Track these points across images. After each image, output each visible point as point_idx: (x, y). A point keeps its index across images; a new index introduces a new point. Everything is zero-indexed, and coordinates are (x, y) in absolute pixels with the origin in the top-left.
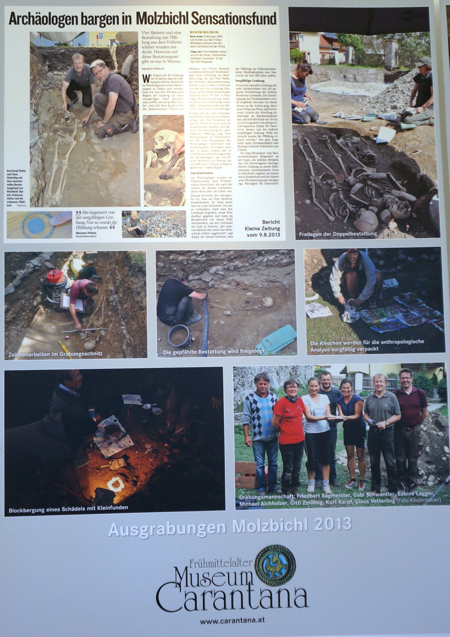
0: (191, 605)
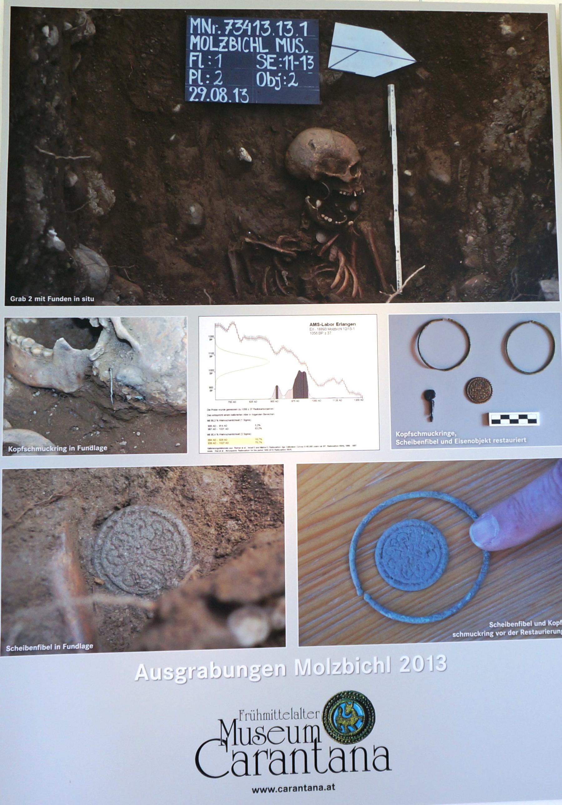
0: (240, 768)
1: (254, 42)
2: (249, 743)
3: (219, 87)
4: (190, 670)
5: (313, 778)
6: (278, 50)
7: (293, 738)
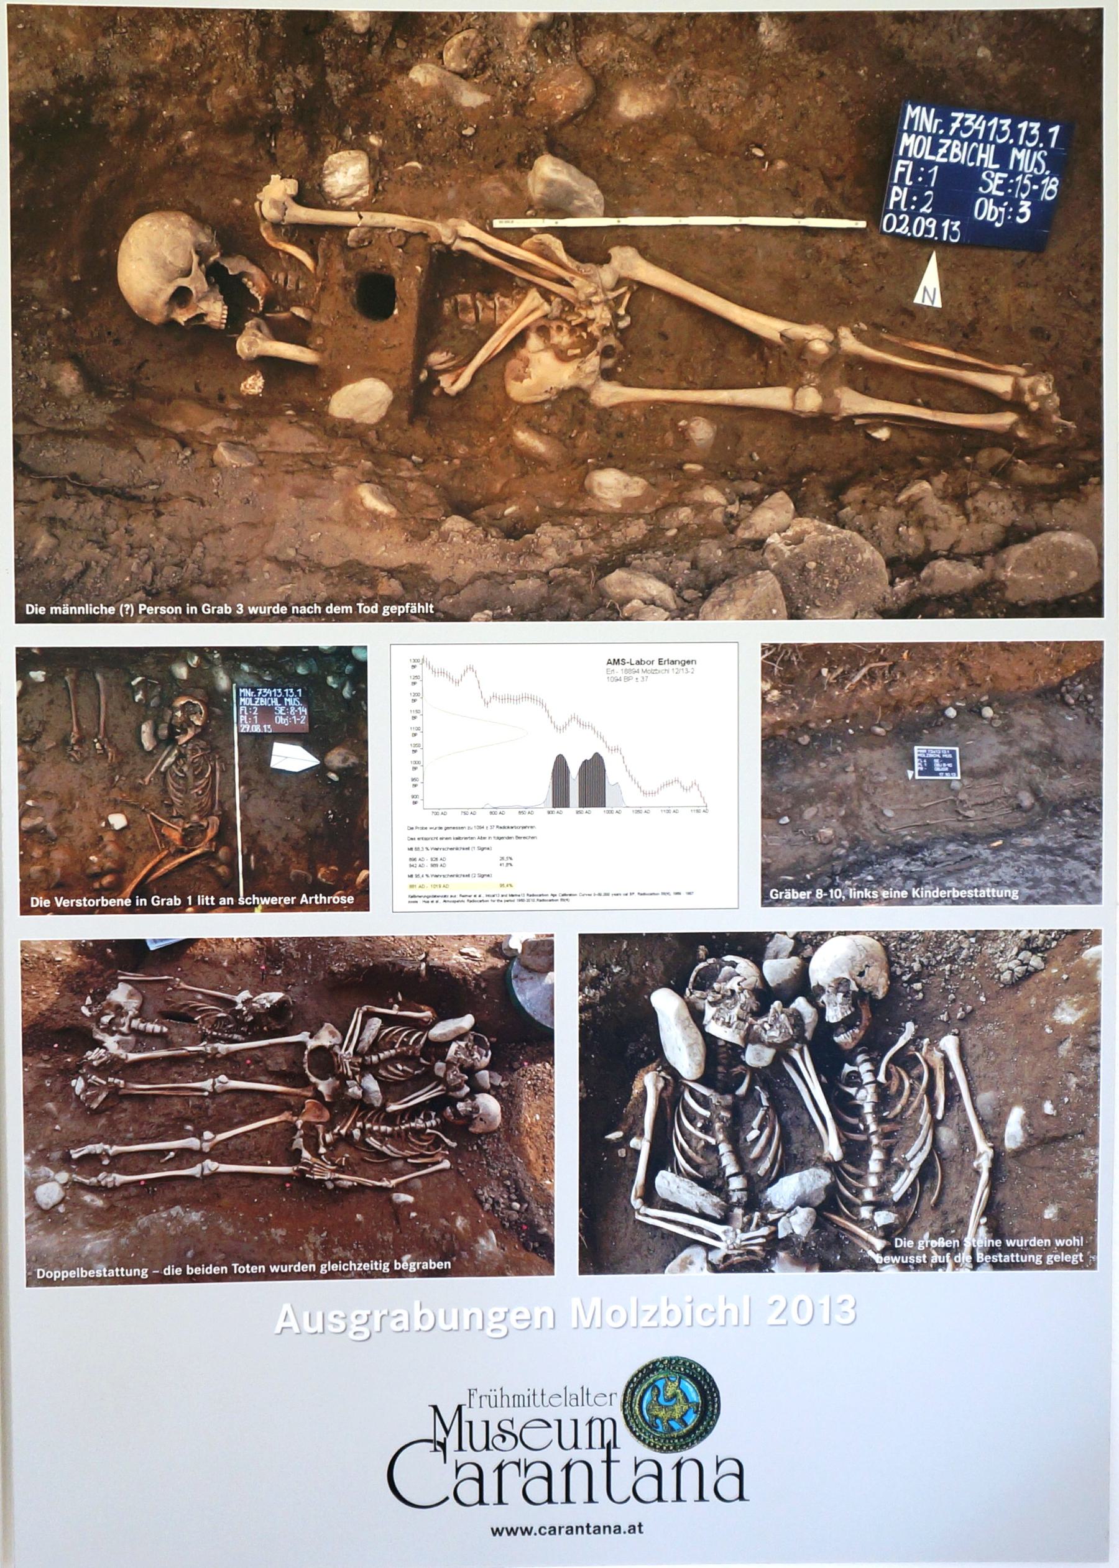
0: (469, 1492)
1: (984, 152)
2: (487, 1447)
3: (926, 216)
4: (377, 1316)
5: (603, 1512)
6: (1011, 167)
7: (568, 1441)
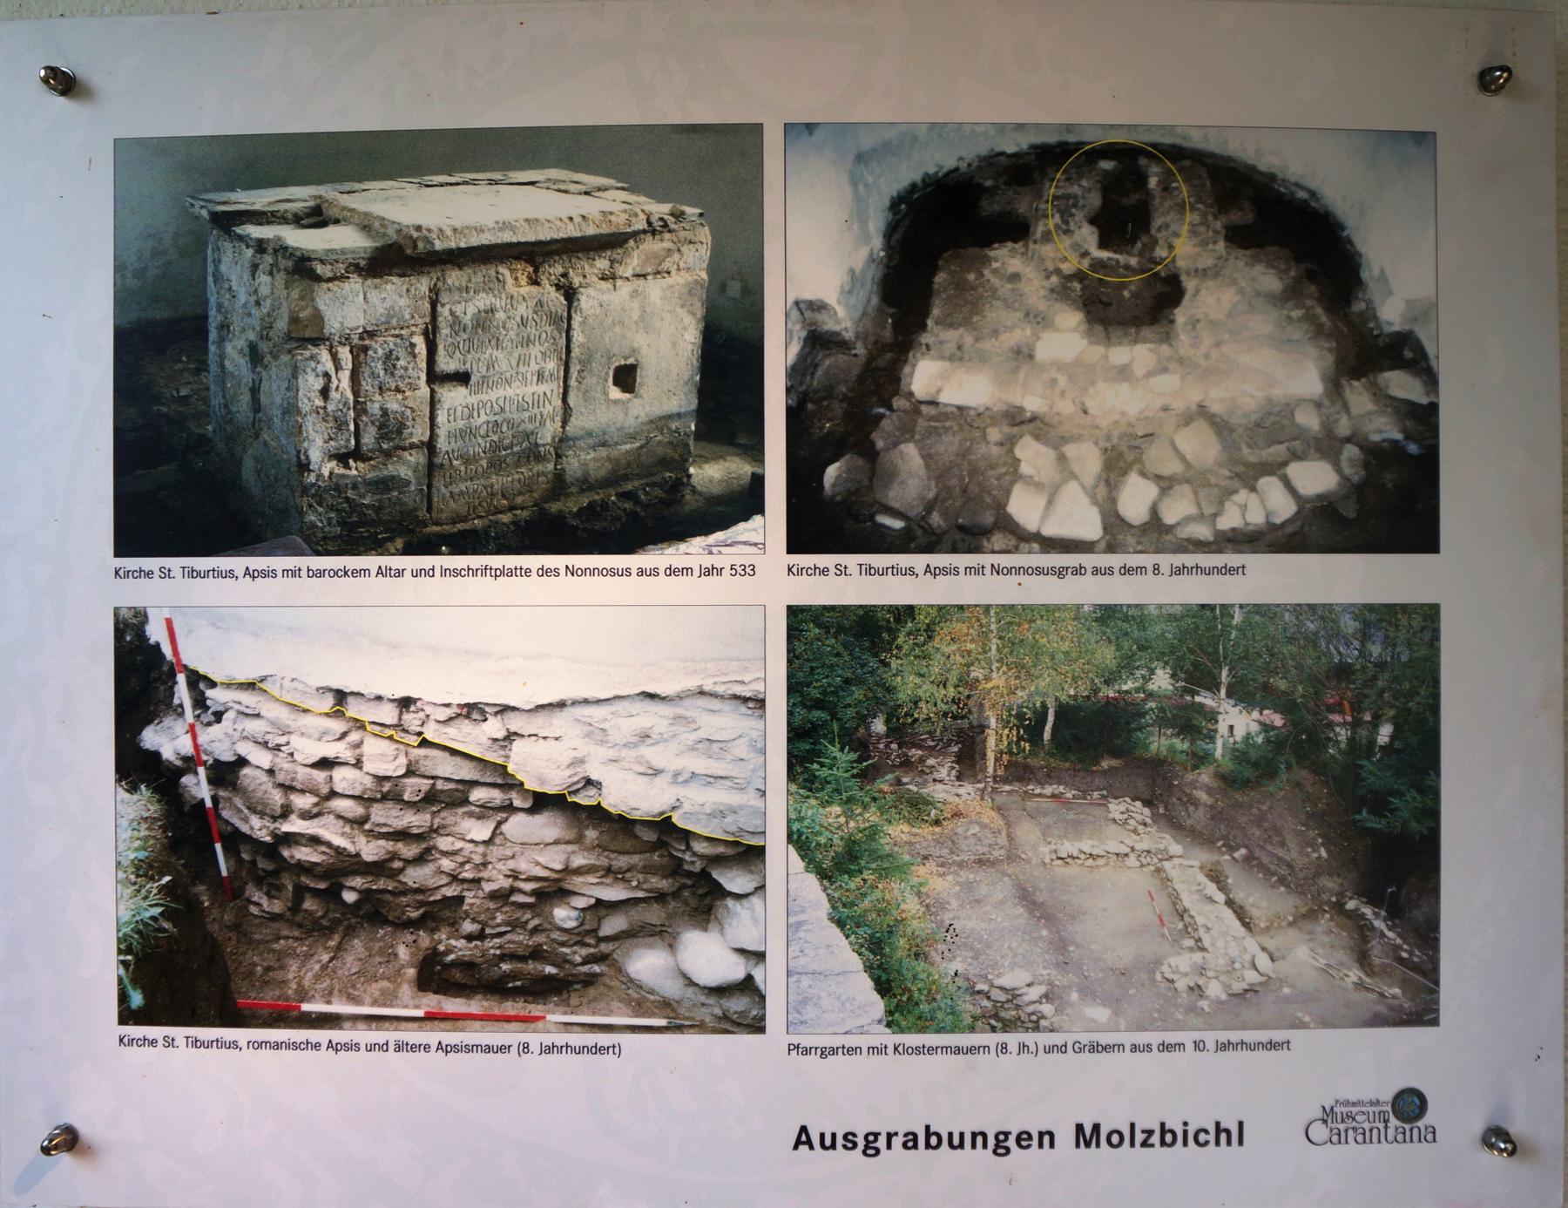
0: (1335, 1139)
